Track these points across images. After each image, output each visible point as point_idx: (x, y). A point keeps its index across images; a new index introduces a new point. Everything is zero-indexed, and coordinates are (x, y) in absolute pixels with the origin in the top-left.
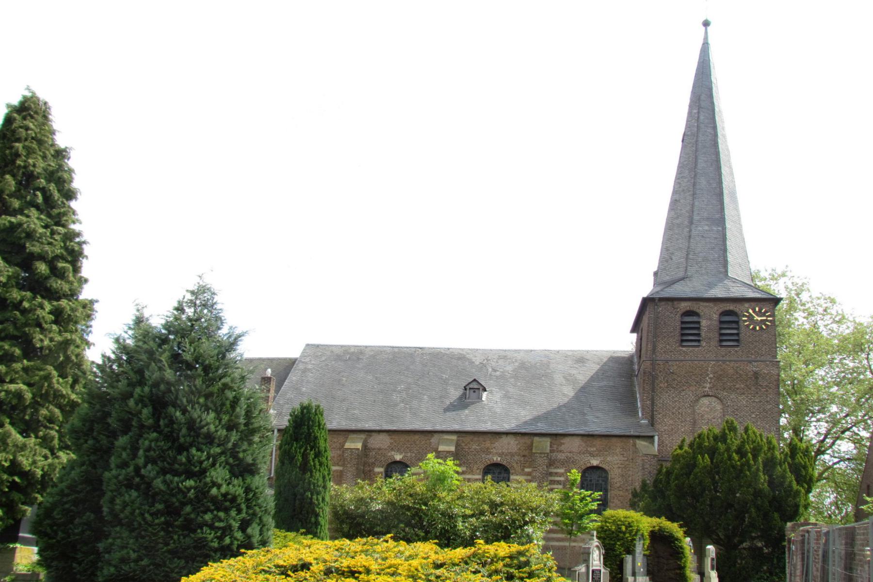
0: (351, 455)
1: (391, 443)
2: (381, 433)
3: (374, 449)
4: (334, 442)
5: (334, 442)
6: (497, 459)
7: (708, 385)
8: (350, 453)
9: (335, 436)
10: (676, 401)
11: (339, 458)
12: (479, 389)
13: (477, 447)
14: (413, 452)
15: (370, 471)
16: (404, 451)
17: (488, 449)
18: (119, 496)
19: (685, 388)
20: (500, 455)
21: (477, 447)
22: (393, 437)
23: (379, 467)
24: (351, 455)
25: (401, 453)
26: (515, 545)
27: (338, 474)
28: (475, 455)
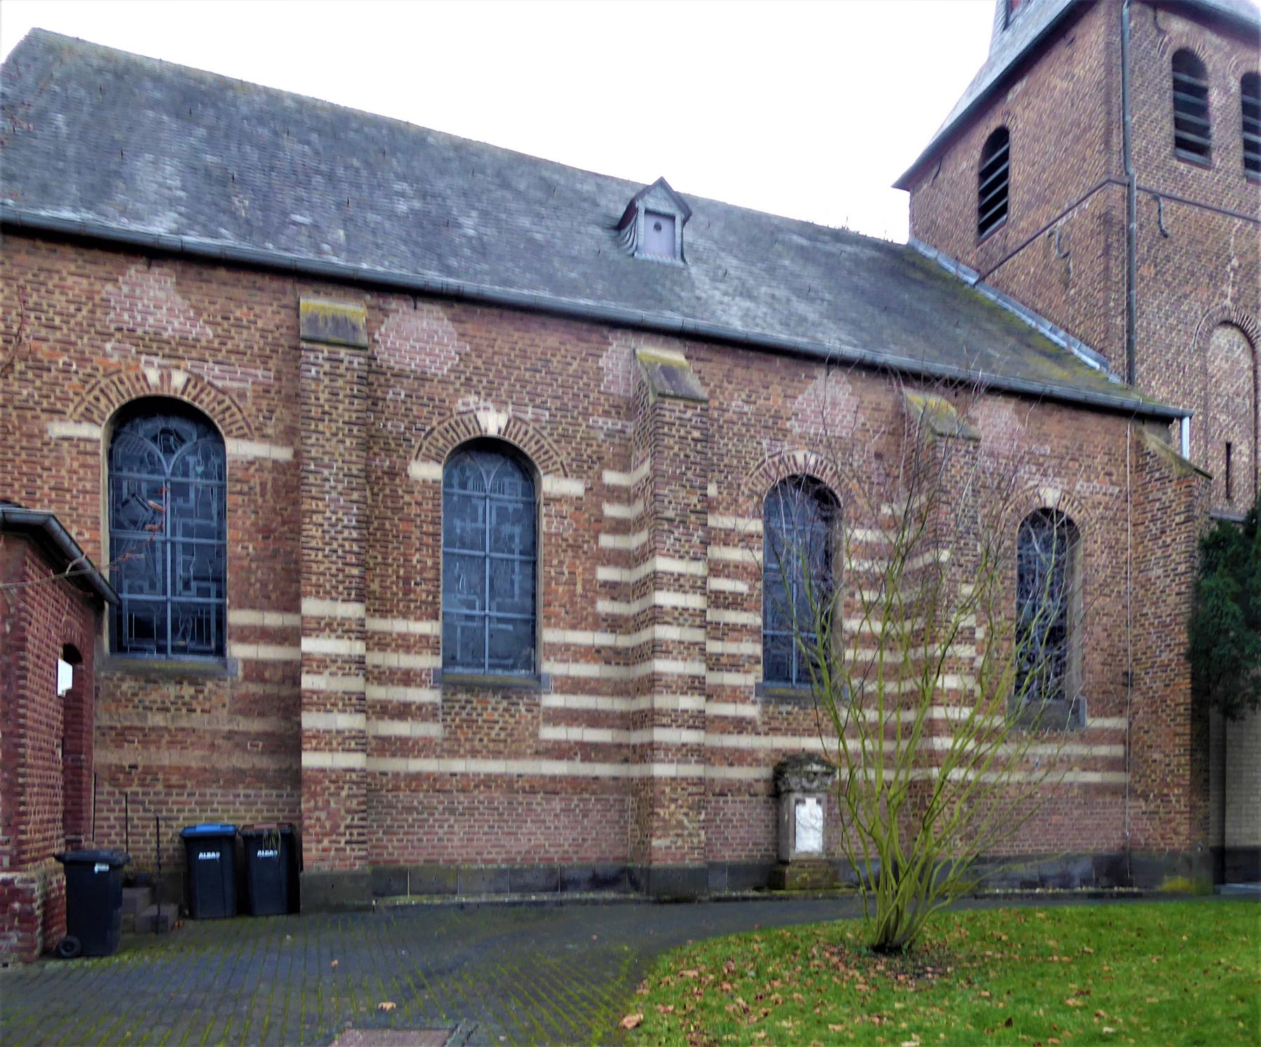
0: (333, 375)
1: (464, 357)
2: (424, 307)
3: (399, 375)
4: (238, 325)
5: (238, 325)
6: (804, 459)
7: (1230, 291)
8: (327, 367)
9: (238, 292)
10: (1172, 328)
11: (264, 404)
12: (672, 218)
13: (746, 409)
14: (542, 406)
15: (392, 474)
16: (510, 394)
17: (777, 417)
18: (769, 951)
19: (1188, 289)
20: (813, 444)
21: (746, 409)
22: (469, 328)
23: (428, 458)
24: (333, 375)
25: (500, 405)
26: (193, 764)
27: (268, 477)
28: (741, 437)
